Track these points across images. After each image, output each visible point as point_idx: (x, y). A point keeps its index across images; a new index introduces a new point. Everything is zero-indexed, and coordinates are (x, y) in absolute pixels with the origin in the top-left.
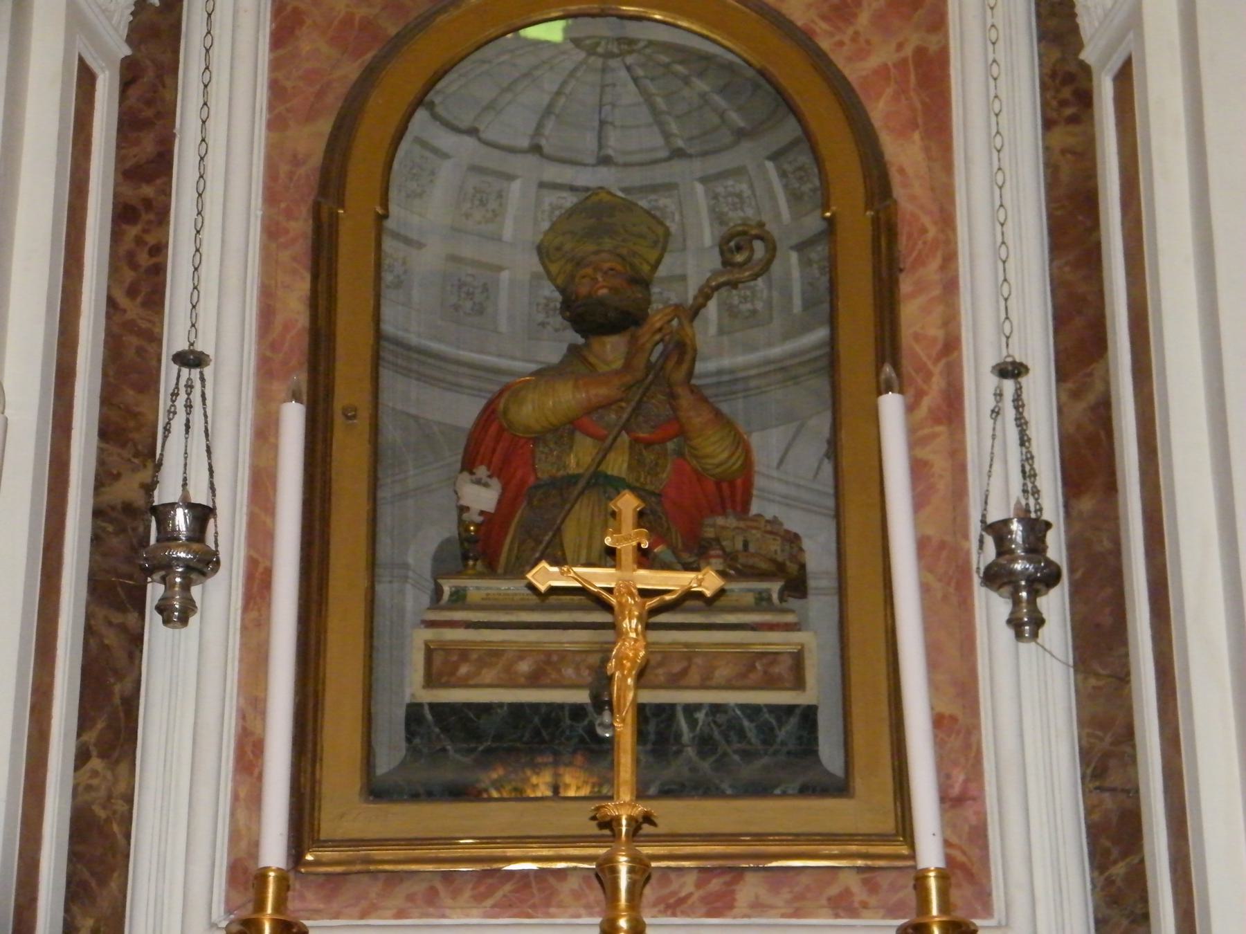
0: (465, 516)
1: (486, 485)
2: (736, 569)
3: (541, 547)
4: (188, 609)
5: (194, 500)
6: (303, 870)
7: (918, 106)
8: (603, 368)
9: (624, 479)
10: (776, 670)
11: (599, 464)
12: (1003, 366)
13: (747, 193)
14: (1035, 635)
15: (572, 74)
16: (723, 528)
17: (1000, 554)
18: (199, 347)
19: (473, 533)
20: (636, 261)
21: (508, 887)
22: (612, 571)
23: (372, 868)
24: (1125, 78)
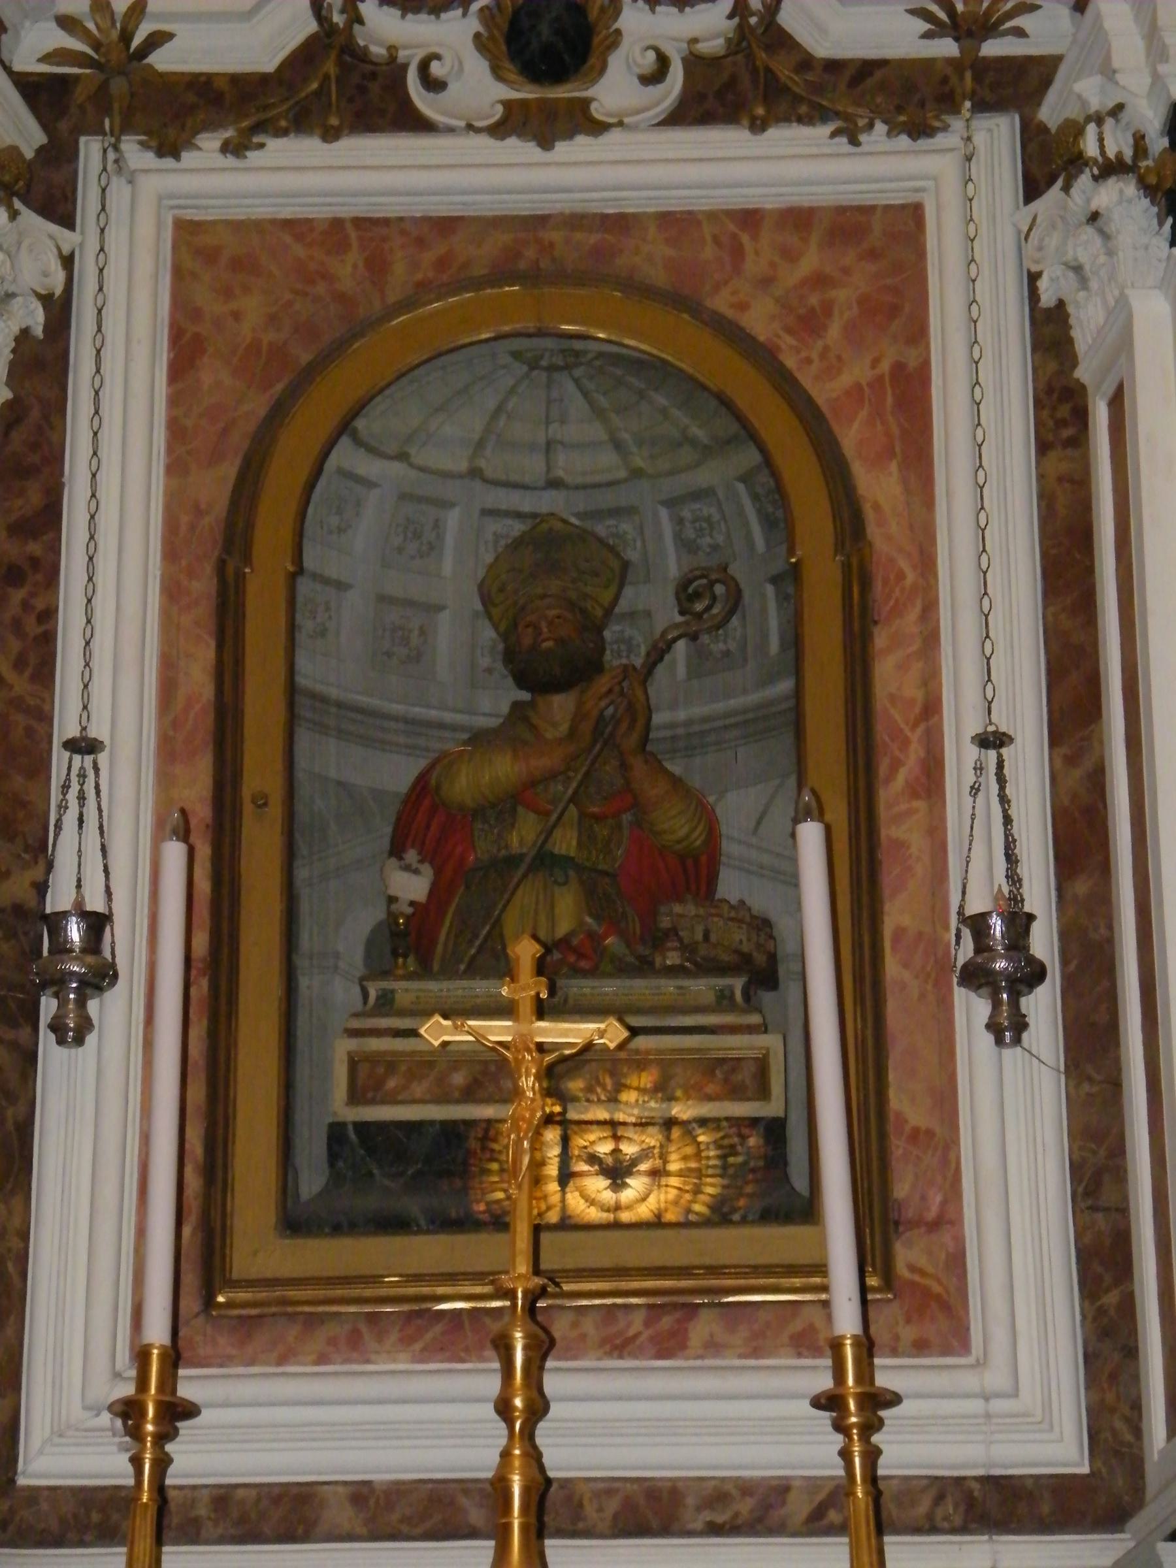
0: (394, 907)
1: (416, 872)
2: (695, 964)
3: (477, 943)
4: (85, 1026)
5: (89, 908)
6: (214, 1313)
7: (895, 431)
8: (550, 734)
9: (572, 859)
10: (738, 1077)
12: (983, 737)
13: (716, 517)
14: (1017, 1041)
15: (512, 391)
16: (681, 916)
17: (978, 950)
18: (92, 733)
20: (589, 605)
21: (438, 1328)
22: (509, 1023)
23: (290, 1309)
24: (1117, 402)
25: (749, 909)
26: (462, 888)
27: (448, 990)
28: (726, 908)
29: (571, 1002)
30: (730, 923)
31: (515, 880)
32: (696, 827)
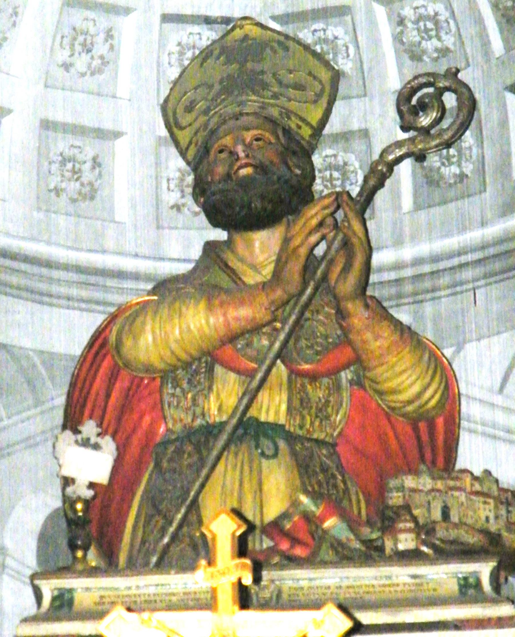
0: (69, 490)
1: (96, 447)
2: (433, 546)
9: (282, 426)
11: (248, 407)
13: (444, 15)
16: (414, 491)
19: (80, 514)
25: (497, 481)
26: (152, 465)
27: (138, 587)
28: (468, 480)
29: (285, 596)
30: (473, 497)
31: (215, 453)
32: (429, 385)
